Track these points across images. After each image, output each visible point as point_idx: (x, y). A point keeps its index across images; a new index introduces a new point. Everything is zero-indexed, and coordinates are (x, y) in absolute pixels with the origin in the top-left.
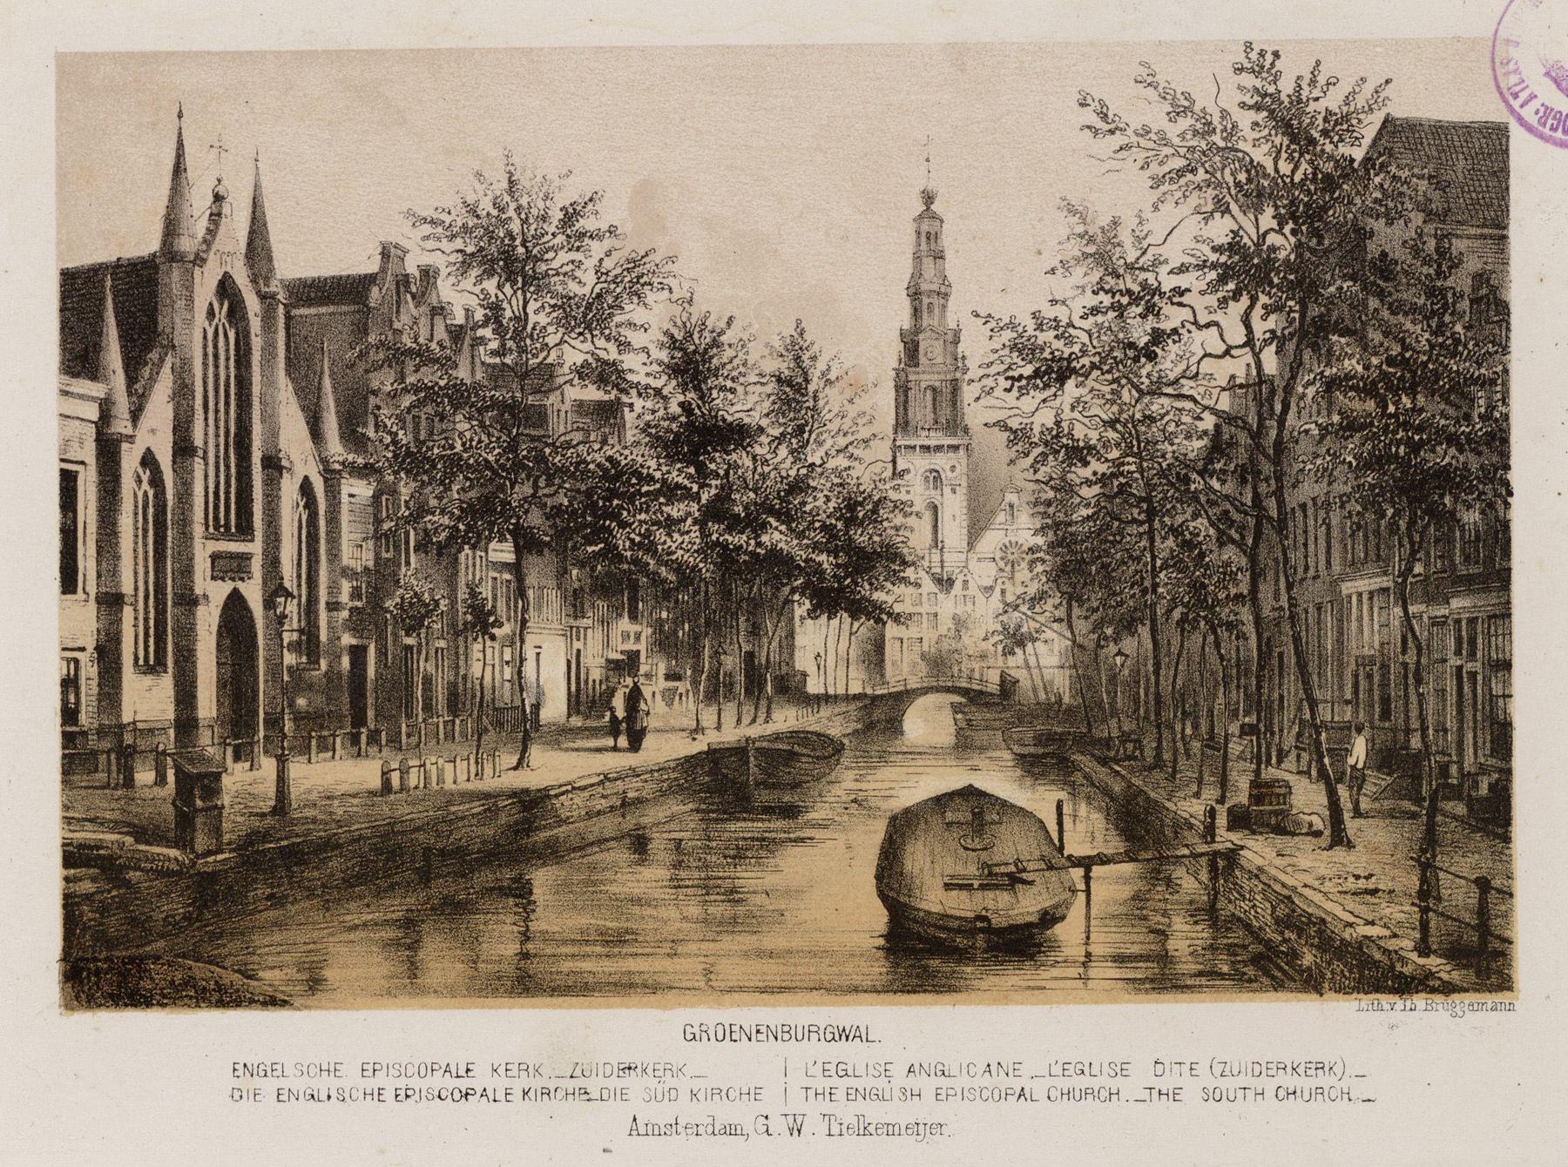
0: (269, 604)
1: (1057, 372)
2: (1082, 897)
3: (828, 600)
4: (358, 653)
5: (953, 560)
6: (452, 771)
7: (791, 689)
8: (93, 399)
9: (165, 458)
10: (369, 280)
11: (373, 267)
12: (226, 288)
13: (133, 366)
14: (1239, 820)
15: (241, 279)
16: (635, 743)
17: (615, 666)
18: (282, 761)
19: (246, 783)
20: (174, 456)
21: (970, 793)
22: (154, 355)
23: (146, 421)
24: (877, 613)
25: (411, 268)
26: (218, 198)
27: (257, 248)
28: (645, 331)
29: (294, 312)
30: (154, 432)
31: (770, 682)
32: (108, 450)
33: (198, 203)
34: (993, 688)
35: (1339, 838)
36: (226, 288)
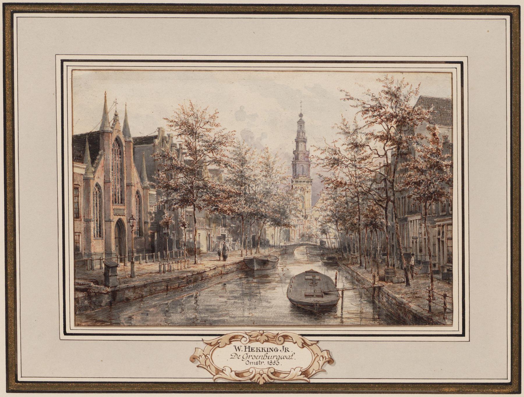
0: (129, 222)
1: (336, 162)
2: (341, 298)
3: (277, 223)
4: (153, 236)
5: (308, 212)
6: (179, 267)
7: (265, 244)
8: (84, 168)
9: (101, 184)
10: (156, 137)
11: (157, 134)
12: (117, 140)
13: (93, 160)
14: (382, 279)
15: (122, 137)
16: (225, 257)
17: (219, 238)
18: (132, 263)
19: (123, 269)
20: (452, 178)
21: (312, 272)
22: (98, 157)
23: (97, 175)
24: (287, 225)
25: (166, 135)
26: (116, 115)
27: (126, 130)
28: (227, 152)
29: (136, 146)
30: (99, 178)
31: (258, 242)
32: (87, 180)
33: (111, 117)
34: (319, 244)
35: (408, 284)
36: (117, 140)
